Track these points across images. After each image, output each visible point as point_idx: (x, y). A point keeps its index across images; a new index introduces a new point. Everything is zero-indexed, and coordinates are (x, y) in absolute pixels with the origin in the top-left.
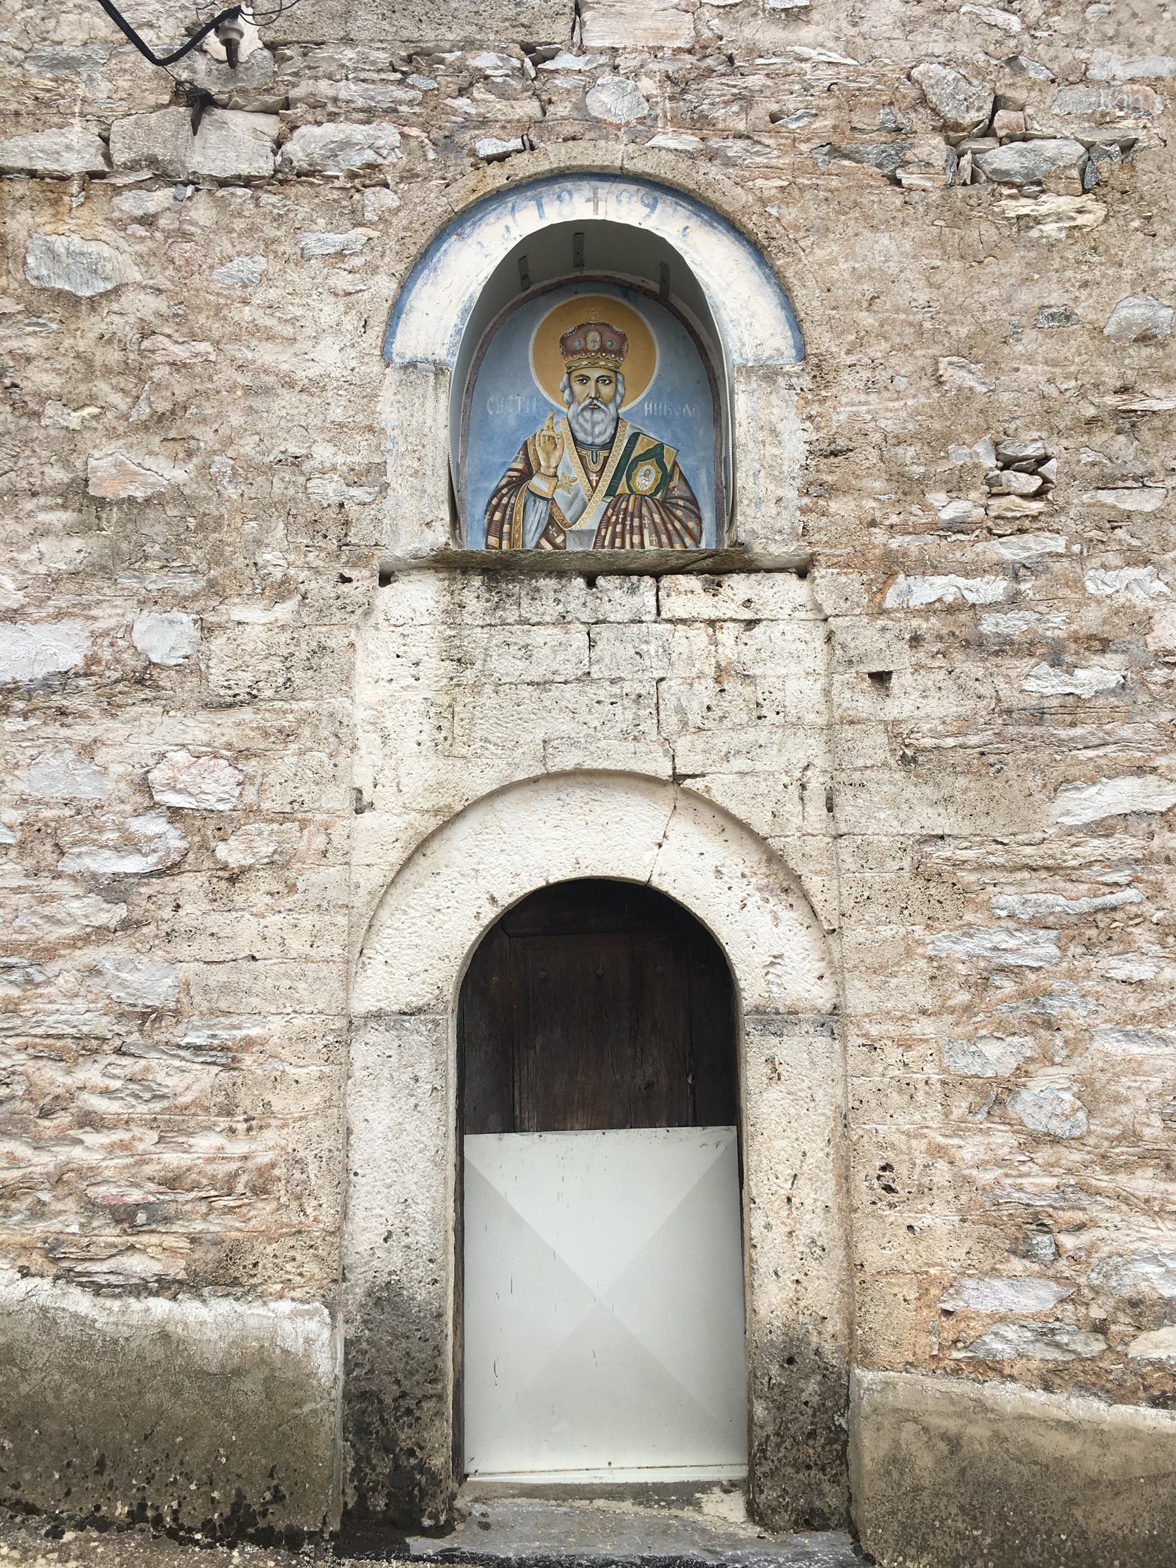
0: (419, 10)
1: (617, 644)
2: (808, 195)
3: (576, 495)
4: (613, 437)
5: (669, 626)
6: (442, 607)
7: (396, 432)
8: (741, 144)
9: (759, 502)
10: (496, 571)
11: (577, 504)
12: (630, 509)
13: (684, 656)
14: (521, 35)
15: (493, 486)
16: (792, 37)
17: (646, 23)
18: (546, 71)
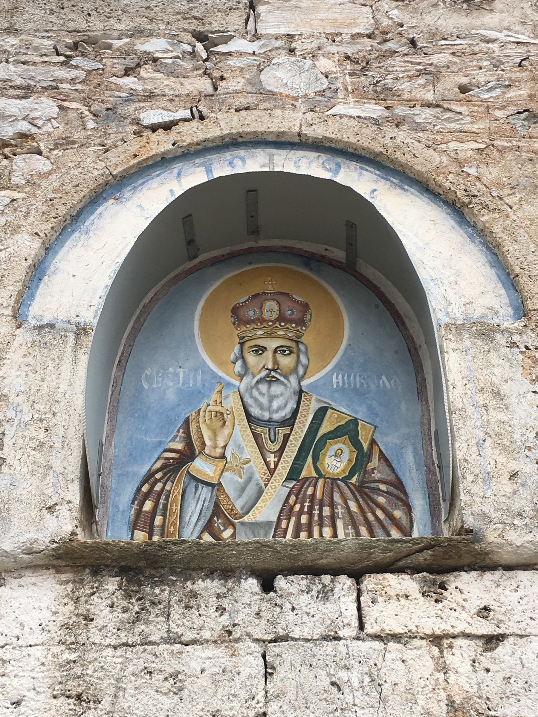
0: (88, 6)
1: (305, 670)
2: (509, 156)
3: (249, 480)
4: (295, 413)
5: (377, 645)
6: (61, 619)
7: (22, 398)
8: (429, 111)
9: (488, 478)
10: (139, 571)
11: (251, 490)
12: (318, 495)
13: (401, 689)
14: (194, 25)
15: (144, 470)
16: (477, 22)
17: (323, 15)
18: (217, 53)
